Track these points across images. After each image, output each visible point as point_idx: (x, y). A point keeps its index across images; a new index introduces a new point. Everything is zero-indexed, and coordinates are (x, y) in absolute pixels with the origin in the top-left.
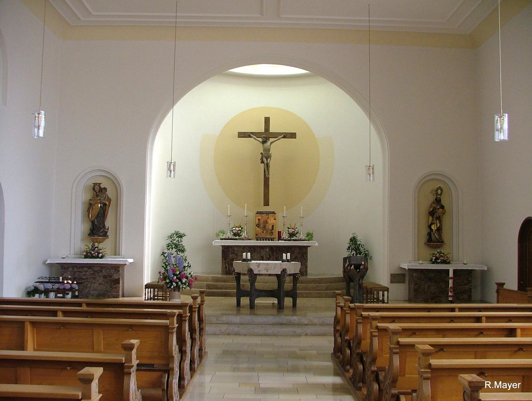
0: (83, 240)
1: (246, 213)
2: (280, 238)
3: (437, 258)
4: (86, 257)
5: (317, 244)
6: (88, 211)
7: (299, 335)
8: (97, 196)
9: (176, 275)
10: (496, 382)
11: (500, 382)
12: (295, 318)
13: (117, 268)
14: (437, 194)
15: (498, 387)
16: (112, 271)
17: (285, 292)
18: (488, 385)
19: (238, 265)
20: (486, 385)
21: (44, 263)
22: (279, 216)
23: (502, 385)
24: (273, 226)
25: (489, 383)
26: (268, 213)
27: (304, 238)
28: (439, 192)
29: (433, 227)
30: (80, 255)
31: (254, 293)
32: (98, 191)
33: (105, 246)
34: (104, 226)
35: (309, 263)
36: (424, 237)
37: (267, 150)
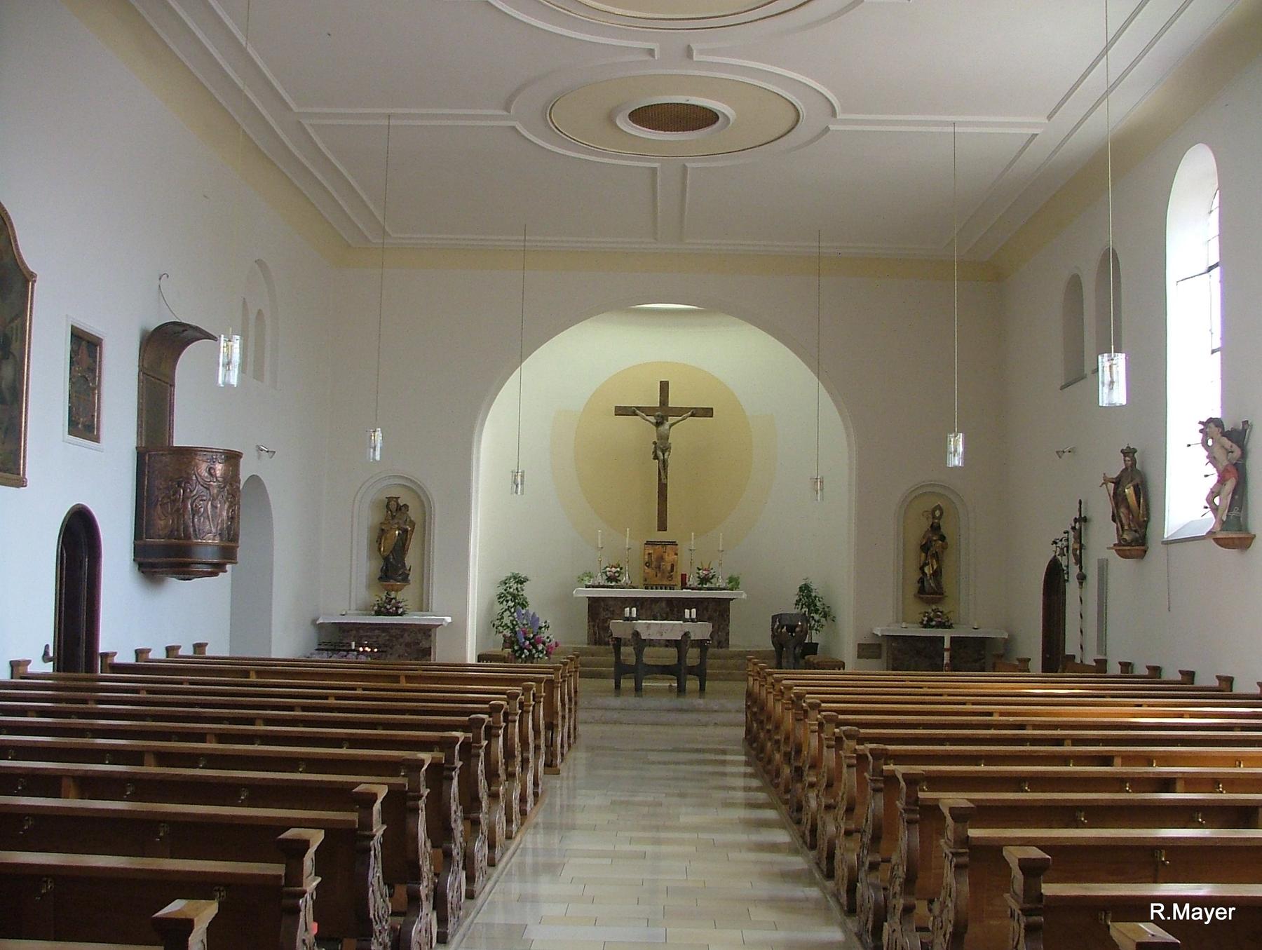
0: (369, 587)
1: (629, 543)
2: (684, 586)
3: (930, 620)
4: (378, 613)
5: (744, 596)
6: (379, 541)
7: (706, 725)
8: (393, 517)
9: (529, 639)
10: (1176, 906)
11: (1187, 906)
12: (701, 701)
13: (426, 631)
14: (934, 517)
15: (1181, 917)
16: (420, 636)
17: (688, 670)
18: (1159, 912)
19: (618, 627)
20: (1153, 911)
21: (314, 622)
22: (683, 548)
23: (1191, 913)
24: (672, 566)
25: (1158, 908)
26: (664, 544)
27: (723, 585)
28: (937, 513)
29: (926, 570)
30: (366, 610)
31: (639, 671)
32: (394, 510)
33: (406, 595)
34: (404, 565)
35: (733, 627)
36: (913, 588)
37: (664, 438)
